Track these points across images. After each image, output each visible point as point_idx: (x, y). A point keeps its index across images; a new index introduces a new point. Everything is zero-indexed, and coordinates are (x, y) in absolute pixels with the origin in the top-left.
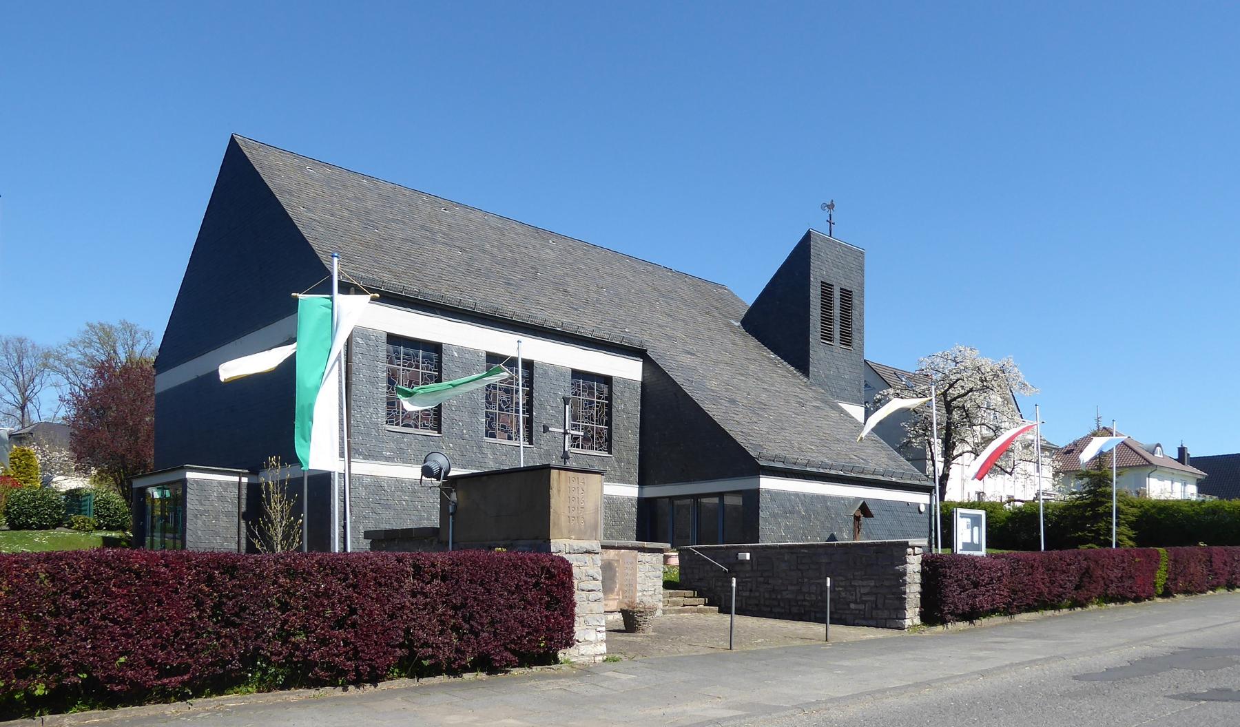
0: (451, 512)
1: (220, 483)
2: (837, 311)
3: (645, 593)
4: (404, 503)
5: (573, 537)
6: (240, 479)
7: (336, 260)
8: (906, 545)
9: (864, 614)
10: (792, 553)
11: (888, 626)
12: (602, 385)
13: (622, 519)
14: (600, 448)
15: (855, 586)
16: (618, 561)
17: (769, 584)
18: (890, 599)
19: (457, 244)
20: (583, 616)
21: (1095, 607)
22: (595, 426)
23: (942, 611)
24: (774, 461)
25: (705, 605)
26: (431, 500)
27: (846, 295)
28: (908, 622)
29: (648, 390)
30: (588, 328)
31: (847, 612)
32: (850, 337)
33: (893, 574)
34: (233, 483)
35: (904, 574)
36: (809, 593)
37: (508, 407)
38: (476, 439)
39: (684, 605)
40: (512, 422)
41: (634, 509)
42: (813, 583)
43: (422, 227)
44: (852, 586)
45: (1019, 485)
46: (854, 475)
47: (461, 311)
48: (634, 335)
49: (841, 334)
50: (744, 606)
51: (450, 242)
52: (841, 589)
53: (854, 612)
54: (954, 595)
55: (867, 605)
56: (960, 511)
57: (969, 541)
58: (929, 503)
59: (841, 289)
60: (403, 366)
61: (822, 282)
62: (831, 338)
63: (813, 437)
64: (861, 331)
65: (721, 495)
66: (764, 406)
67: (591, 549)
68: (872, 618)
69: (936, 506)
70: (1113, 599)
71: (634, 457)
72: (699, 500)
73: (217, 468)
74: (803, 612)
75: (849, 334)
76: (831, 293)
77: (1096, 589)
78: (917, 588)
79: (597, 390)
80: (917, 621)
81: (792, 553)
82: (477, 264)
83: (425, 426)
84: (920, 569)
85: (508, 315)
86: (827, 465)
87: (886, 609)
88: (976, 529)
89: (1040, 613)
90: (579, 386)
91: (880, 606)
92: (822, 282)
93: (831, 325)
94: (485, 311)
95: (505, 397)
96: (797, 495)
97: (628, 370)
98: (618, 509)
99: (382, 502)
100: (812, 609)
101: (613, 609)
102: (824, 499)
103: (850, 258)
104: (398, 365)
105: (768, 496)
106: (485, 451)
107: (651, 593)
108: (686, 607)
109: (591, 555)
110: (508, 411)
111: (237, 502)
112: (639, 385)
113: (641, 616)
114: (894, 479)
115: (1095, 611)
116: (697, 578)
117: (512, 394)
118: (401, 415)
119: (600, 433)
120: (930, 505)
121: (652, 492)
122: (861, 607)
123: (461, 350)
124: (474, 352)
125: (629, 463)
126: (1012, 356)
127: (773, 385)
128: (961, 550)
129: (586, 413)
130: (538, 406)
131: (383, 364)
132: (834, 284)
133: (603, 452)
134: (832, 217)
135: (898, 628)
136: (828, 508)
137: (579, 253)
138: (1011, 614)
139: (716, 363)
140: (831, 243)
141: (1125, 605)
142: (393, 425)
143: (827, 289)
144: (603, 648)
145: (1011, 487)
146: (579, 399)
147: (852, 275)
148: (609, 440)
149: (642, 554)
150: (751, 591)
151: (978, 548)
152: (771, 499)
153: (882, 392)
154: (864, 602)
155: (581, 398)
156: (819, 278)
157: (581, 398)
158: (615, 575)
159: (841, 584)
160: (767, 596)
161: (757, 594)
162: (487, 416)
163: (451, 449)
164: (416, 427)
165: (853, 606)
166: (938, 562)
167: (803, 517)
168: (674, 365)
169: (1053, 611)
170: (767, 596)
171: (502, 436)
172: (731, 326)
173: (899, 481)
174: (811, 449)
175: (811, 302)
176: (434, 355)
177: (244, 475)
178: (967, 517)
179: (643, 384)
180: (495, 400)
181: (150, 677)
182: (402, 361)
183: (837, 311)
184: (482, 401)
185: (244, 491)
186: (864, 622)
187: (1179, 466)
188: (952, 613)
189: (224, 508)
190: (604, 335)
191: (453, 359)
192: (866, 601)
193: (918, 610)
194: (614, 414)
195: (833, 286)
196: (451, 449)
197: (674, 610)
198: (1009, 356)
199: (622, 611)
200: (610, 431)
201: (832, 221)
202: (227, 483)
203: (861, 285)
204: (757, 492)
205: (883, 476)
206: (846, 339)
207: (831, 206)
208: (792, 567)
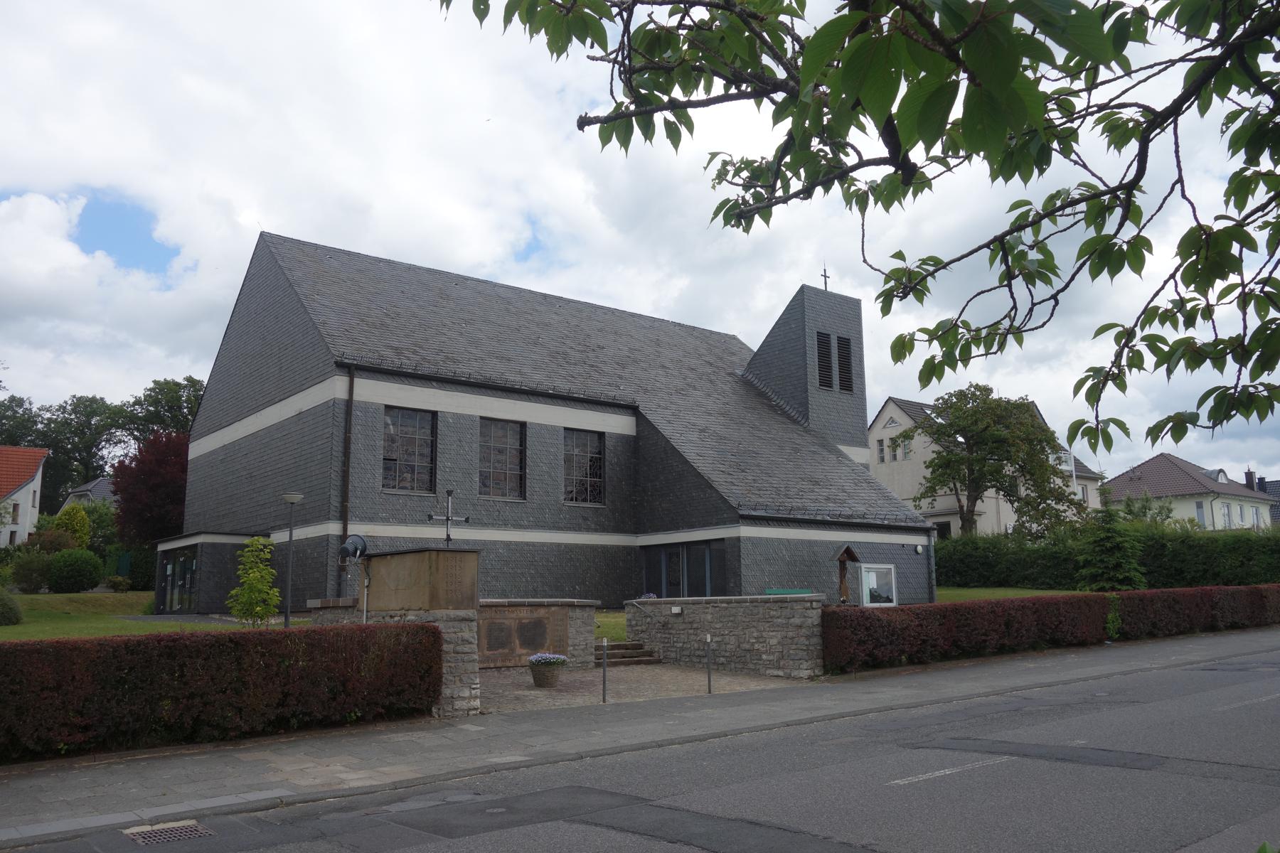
0: (366, 585)
3: (576, 647)
5: (451, 607)
16: (548, 618)
20: (458, 676)
46: (842, 520)
48: (625, 393)
59: (838, 337)
61: (818, 332)
83: (420, 488)
92: (818, 332)
96: (780, 541)
102: (811, 543)
107: (582, 647)
132: (830, 333)
142: (389, 488)
162: (481, 475)
164: (413, 489)
165: (764, 657)
181: (1247, 622)
187: (1248, 492)
195: (829, 335)
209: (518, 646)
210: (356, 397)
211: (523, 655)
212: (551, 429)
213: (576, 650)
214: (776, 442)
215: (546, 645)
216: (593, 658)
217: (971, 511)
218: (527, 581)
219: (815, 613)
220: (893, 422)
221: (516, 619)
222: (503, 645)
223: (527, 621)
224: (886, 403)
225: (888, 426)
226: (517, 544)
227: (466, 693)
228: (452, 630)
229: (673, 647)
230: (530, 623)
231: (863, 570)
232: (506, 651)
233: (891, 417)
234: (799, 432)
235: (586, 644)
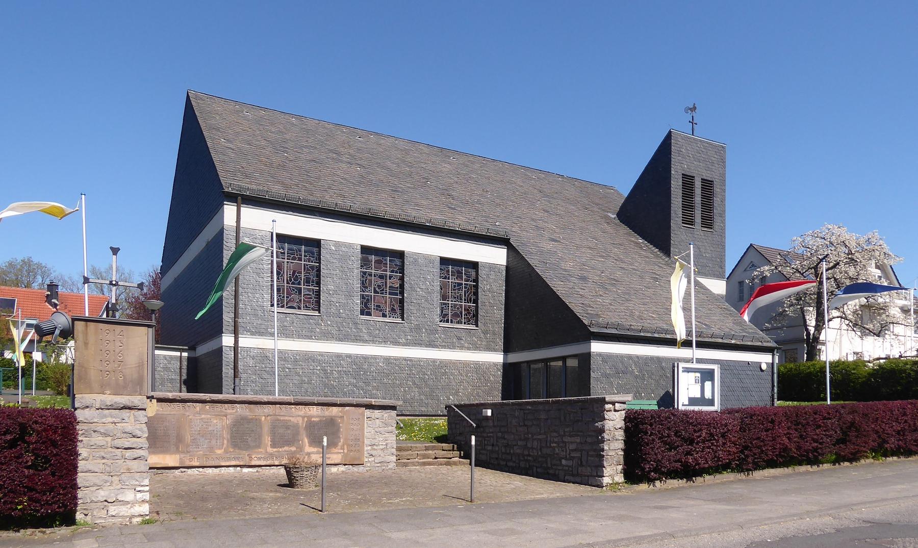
1: (165, 356)
2: (698, 199)
3: (375, 447)
4: (287, 370)
5: (108, 392)
6: (181, 354)
7: (692, 246)
8: (603, 401)
9: (572, 471)
10: (520, 409)
11: (590, 483)
12: (470, 270)
13: (488, 381)
14: (468, 322)
15: (565, 443)
16: (342, 417)
17: (505, 439)
18: (592, 456)
19: (359, 162)
21: (871, 460)
22: (463, 304)
23: (643, 469)
24: (606, 328)
25: (460, 457)
26: (311, 368)
27: (708, 185)
28: (606, 480)
29: (511, 273)
30: (459, 222)
31: (560, 468)
32: (711, 221)
33: (594, 431)
34: (176, 357)
35: (602, 431)
36: (532, 448)
37: (383, 290)
38: (352, 317)
39: (436, 458)
40: (386, 302)
41: (499, 373)
42: (535, 439)
43: (331, 151)
44: (563, 442)
45: (887, 344)
47: (446, 230)
48: (500, 227)
49: (702, 219)
50: (488, 460)
51: (353, 161)
52: (555, 445)
53: (565, 468)
54: (656, 450)
55: (574, 461)
56: (682, 365)
57: (698, 395)
58: (771, 362)
59: (702, 179)
60: (287, 259)
61: (683, 174)
62: (693, 222)
63: (658, 307)
64: (722, 215)
65: (564, 359)
66: (615, 282)
67: (130, 405)
68: (578, 475)
69: (699, 361)
70: (896, 452)
71: (500, 329)
72: (548, 364)
73: (162, 346)
74: (528, 467)
75: (711, 218)
76: (692, 184)
77: (866, 443)
78: (620, 445)
79: (465, 274)
80: (620, 478)
81: (520, 409)
82: (371, 177)
83: (307, 308)
84: (624, 426)
85: (381, 215)
86: (663, 330)
87: (589, 466)
88: (708, 384)
89: (790, 468)
90: (448, 271)
91: (584, 463)
93: (693, 211)
94: (364, 212)
95: (380, 282)
96: (630, 357)
97: (496, 256)
98: (485, 372)
99: (268, 369)
100: (535, 464)
101: (336, 462)
103: (711, 152)
104: (282, 258)
105: (600, 359)
106: (360, 326)
107: (381, 447)
108: (438, 459)
109: (133, 412)
110: (382, 293)
111: (179, 371)
112: (504, 269)
113: (297, 472)
114: (733, 342)
115: (847, 467)
116: (458, 432)
117: (386, 279)
118: (285, 299)
119: (468, 310)
120: (773, 364)
121: (514, 358)
122: (570, 463)
123: (338, 244)
124: (350, 246)
125: (494, 334)
126: (877, 231)
127: (632, 264)
128: (683, 405)
129: (455, 293)
130: (410, 289)
131: (268, 258)
133: (471, 325)
134: (694, 118)
135: (598, 486)
136: (662, 368)
137: (476, 166)
138: (748, 470)
139: (578, 247)
140: (692, 140)
141: (908, 459)
143: (688, 181)
144: (145, 509)
145: (880, 347)
146: (449, 282)
147: (713, 167)
148: (476, 315)
149: (371, 410)
150: (493, 445)
151: (711, 402)
152: (602, 361)
153: (759, 269)
154: (572, 458)
155: (450, 281)
156: (679, 171)
157: (450, 281)
158: (338, 430)
159: (556, 440)
160: (503, 450)
161: (497, 449)
163: (328, 325)
164: (299, 308)
165: (564, 462)
166: (639, 418)
167: (636, 377)
168: (534, 250)
169: (809, 466)
170: (503, 450)
171: (377, 315)
172: (607, 217)
173: (738, 343)
174: (653, 317)
175: (672, 192)
176: (315, 250)
177: (184, 350)
178: (695, 372)
179: (508, 268)
180: (370, 285)
182: (286, 255)
183: (698, 199)
184: (358, 286)
185: (185, 363)
186: (571, 478)
188: (656, 470)
189: (168, 377)
190: (471, 228)
191: (331, 253)
192: (574, 457)
193: (620, 467)
194: (480, 294)
195: (694, 177)
196: (328, 325)
197: (418, 462)
198: (875, 231)
199: (286, 467)
200: (477, 307)
201: (695, 122)
202: (171, 357)
203: (723, 176)
204: (589, 355)
205: (722, 338)
206: (708, 222)
207: (694, 109)
208: (521, 424)
209: (307, 444)
210: (243, 224)
211: (313, 453)
212: (428, 259)
213: (375, 449)
214: (637, 272)
215: (340, 444)
216: (394, 458)
217: (816, 339)
218: (405, 391)
219: (617, 416)
220: (753, 265)
221: (303, 417)
222: (289, 443)
223: (317, 419)
224: (748, 249)
225: (748, 269)
226: (396, 359)
227: (129, 496)
228: (110, 420)
229: (485, 449)
230: (320, 421)
231: (681, 369)
232: (293, 449)
233: (752, 262)
234: (661, 265)
235: (387, 445)
